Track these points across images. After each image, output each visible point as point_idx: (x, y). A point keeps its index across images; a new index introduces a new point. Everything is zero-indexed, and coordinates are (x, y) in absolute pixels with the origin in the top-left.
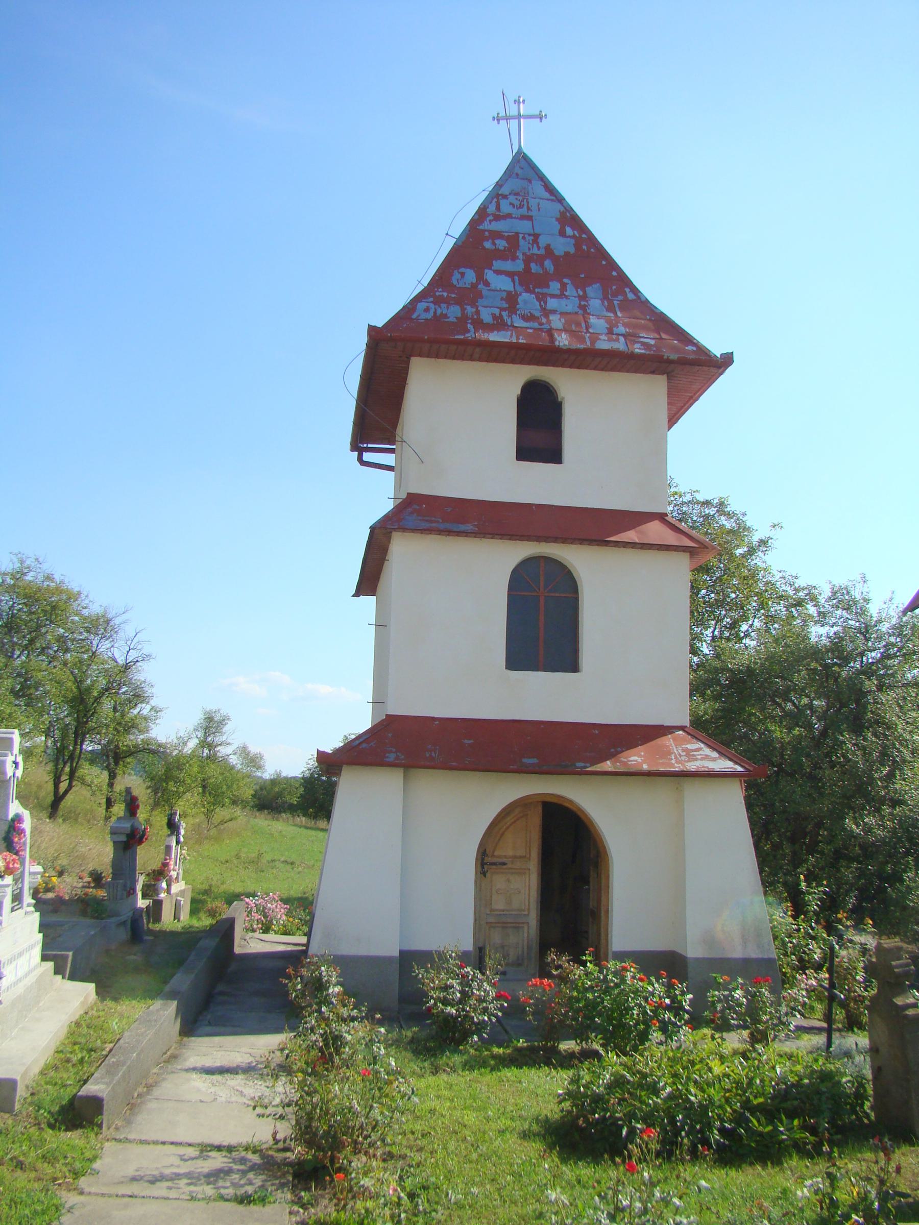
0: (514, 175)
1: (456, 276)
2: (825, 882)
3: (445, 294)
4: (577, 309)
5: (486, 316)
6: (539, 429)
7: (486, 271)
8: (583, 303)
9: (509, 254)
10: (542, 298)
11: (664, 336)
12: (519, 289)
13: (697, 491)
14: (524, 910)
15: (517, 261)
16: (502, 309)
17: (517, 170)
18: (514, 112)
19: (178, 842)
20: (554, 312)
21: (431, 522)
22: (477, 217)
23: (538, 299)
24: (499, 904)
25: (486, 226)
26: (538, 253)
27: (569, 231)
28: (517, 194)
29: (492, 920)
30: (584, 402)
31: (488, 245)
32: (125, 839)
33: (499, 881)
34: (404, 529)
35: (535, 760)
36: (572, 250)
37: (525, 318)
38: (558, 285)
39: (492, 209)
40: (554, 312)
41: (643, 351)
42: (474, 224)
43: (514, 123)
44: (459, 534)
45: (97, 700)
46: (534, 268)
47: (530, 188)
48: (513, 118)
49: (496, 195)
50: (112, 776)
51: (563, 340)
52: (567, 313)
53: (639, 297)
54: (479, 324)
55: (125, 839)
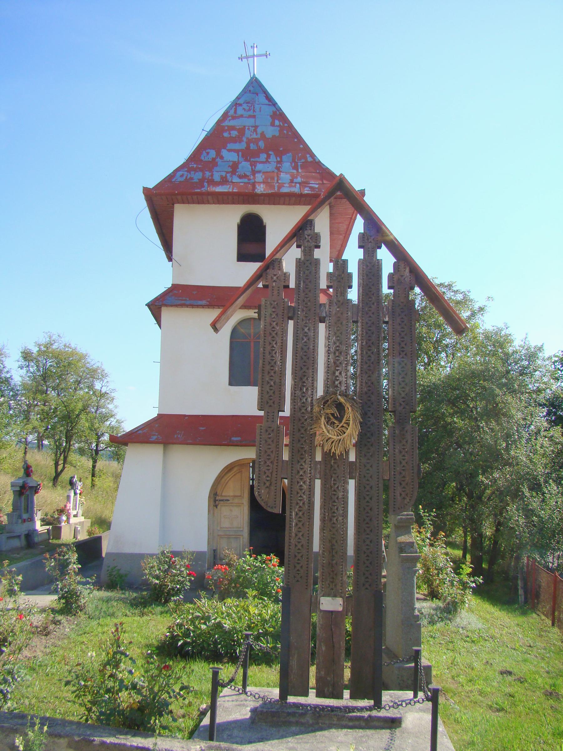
0: (248, 91)
1: (204, 153)
2: (434, 510)
3: (195, 166)
4: (274, 169)
5: (217, 178)
7: (223, 150)
8: (278, 165)
9: (238, 139)
10: (253, 164)
11: (325, 182)
12: (241, 159)
13: (436, 278)
14: (240, 528)
15: (243, 143)
16: (227, 172)
17: (251, 88)
18: (251, 54)
19: (75, 494)
20: (259, 172)
21: (182, 300)
22: (221, 118)
23: (251, 165)
24: (226, 524)
25: (226, 123)
26: (256, 137)
27: (277, 123)
28: (248, 103)
29: (220, 533)
31: (226, 135)
32: (19, 489)
33: (224, 510)
34: (166, 305)
35: (239, 439)
36: (277, 134)
37: (240, 177)
38: (265, 156)
39: (232, 112)
40: (259, 172)
41: (310, 192)
42: (219, 122)
43: (251, 60)
44: (198, 306)
45: (78, 416)
46: (253, 147)
47: (257, 99)
48: (251, 57)
49: (235, 104)
50: (95, 462)
51: (260, 189)
52: (267, 172)
53: (314, 160)
54: (212, 182)
55: (19, 489)
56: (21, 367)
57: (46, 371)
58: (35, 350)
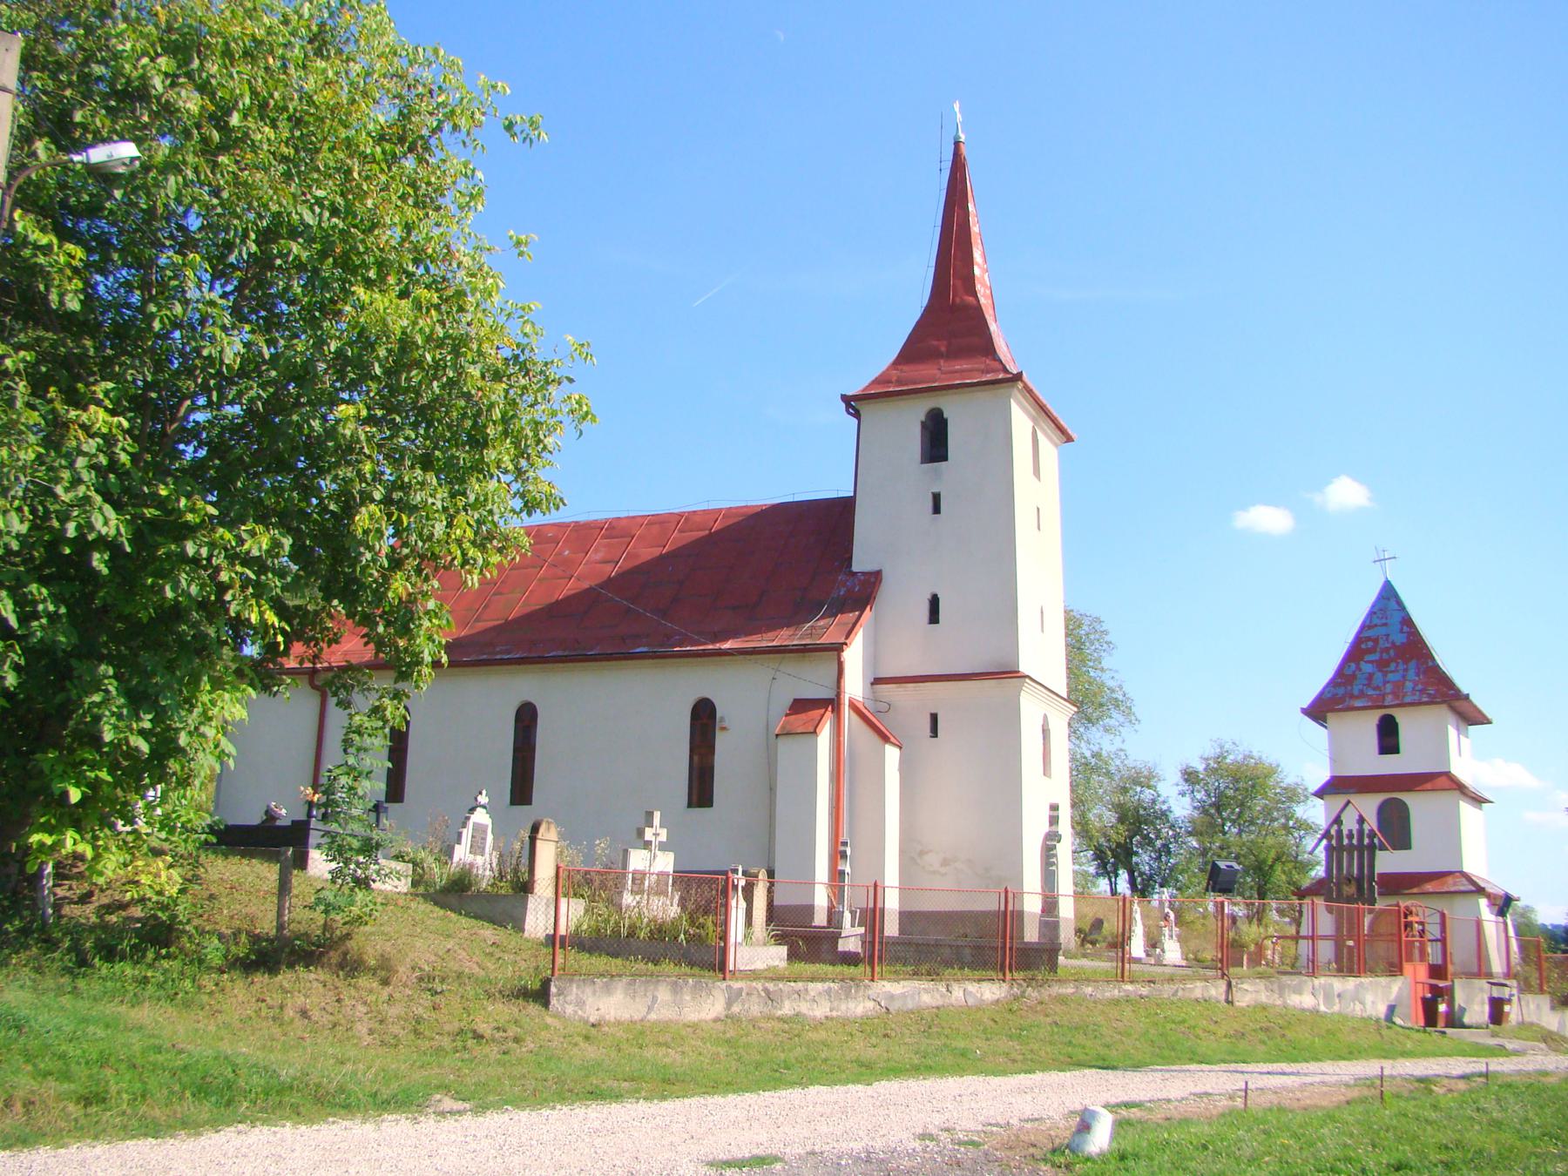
5: (1356, 692)
6: (1388, 738)
9: (1371, 651)
25: (1365, 634)
30: (1410, 724)
45: (1271, 867)
49: (1371, 613)
56: (1183, 794)
57: (1220, 795)
58: (1200, 767)
